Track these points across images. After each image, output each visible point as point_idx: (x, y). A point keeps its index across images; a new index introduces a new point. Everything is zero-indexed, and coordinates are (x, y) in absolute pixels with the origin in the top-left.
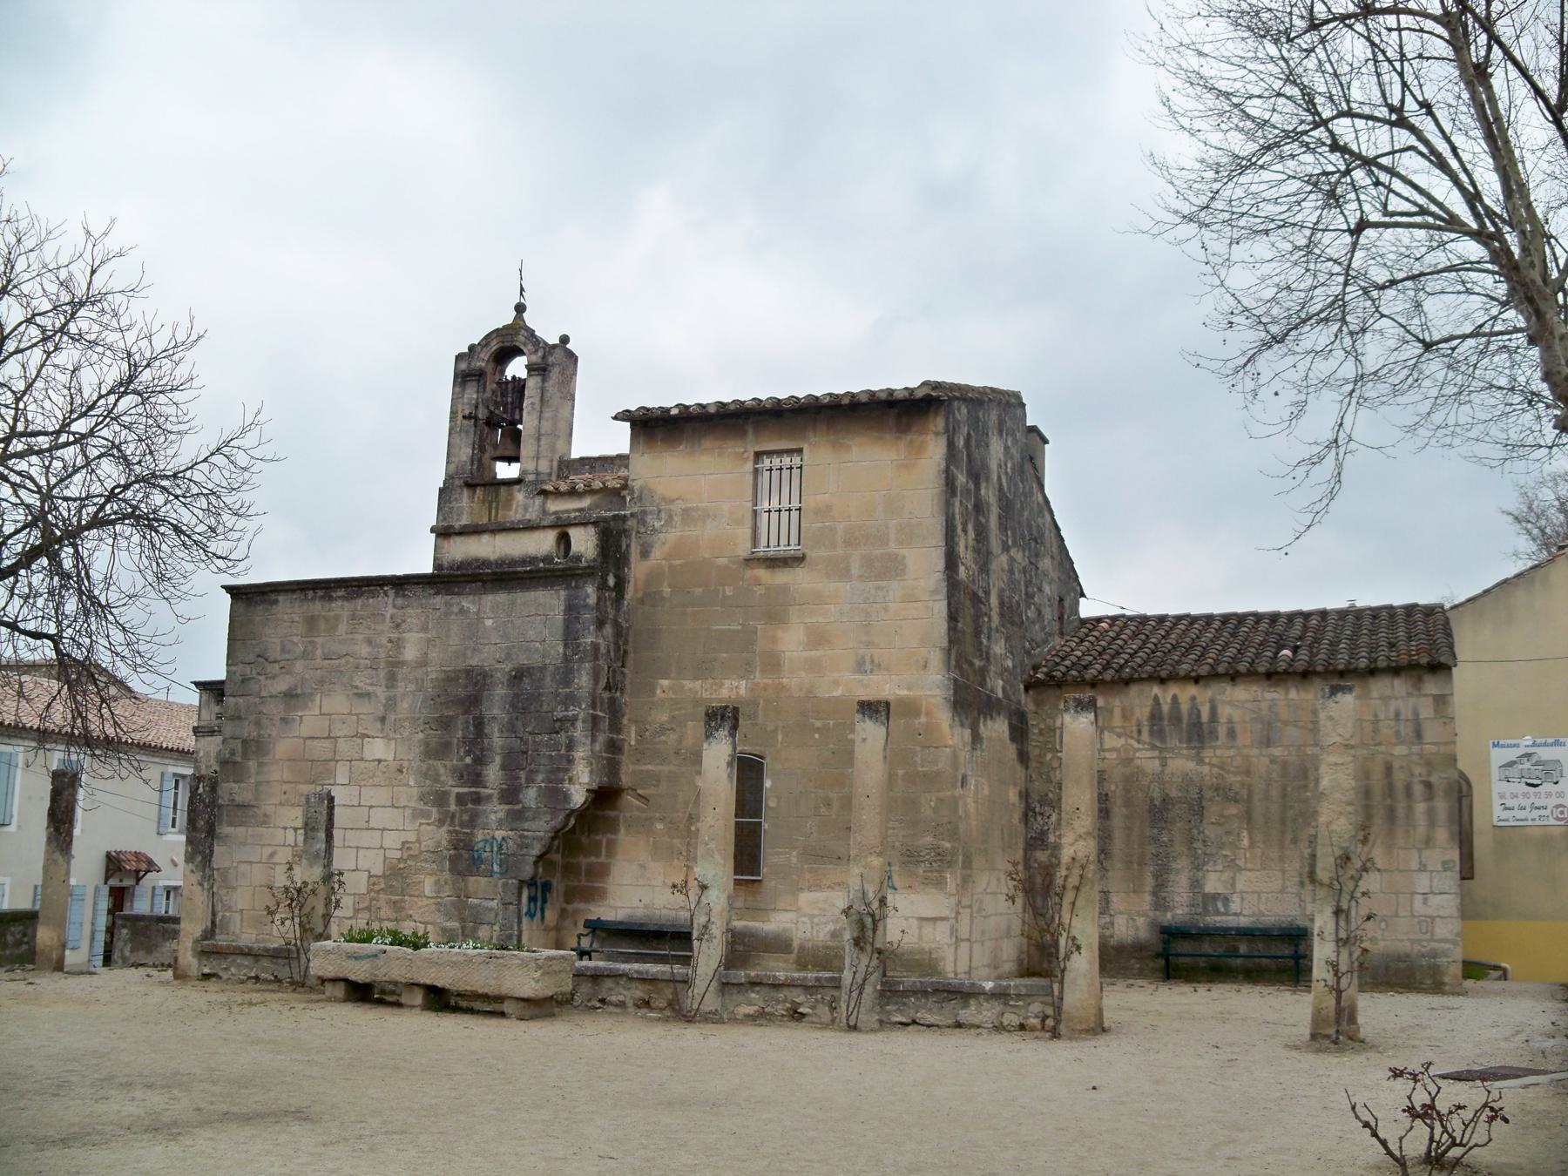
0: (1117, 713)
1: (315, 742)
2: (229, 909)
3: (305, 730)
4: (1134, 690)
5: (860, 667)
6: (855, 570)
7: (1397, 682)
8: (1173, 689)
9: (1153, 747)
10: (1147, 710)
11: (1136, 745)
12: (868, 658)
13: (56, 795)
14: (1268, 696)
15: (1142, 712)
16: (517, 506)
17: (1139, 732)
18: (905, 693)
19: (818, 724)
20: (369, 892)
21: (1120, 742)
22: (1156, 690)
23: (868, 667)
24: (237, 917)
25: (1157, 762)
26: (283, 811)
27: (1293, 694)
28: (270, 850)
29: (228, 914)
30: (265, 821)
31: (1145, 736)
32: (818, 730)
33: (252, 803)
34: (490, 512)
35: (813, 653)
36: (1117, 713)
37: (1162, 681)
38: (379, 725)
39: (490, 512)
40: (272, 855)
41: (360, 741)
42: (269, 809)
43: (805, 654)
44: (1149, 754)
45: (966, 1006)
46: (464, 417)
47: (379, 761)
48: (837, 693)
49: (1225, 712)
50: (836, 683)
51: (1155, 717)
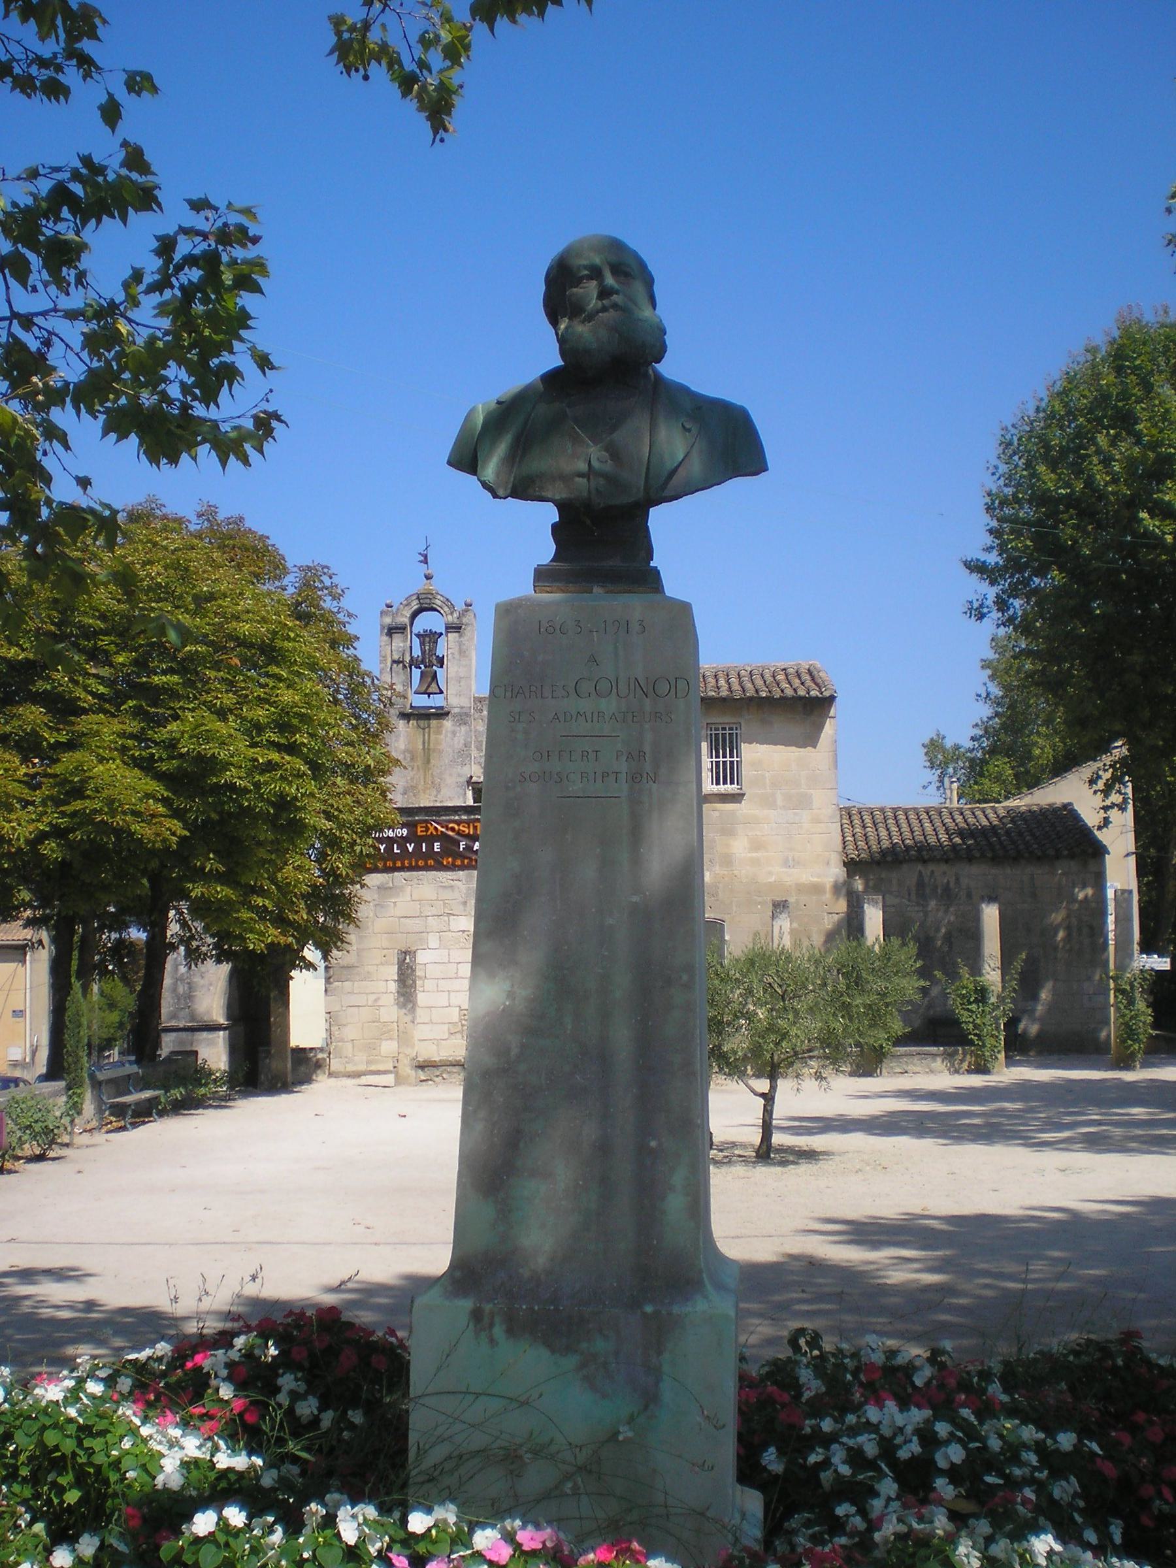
0: (894, 882)
1: (408, 920)
2: (342, 1040)
3: (398, 912)
4: (905, 867)
5: (786, 863)
6: (779, 802)
7: (1072, 863)
8: (931, 867)
9: (918, 904)
10: (914, 881)
11: (907, 903)
12: (790, 858)
13: (401, 963)
14: (993, 871)
15: (912, 881)
16: (447, 732)
17: (909, 894)
18: (816, 879)
19: (760, 899)
20: (461, 1020)
21: (897, 901)
22: (920, 867)
23: (791, 863)
24: (349, 1045)
25: (922, 914)
26: (382, 969)
27: (1008, 871)
28: (373, 997)
29: (340, 1044)
30: (367, 977)
31: (913, 897)
32: (760, 903)
33: (356, 965)
34: (424, 735)
35: (754, 855)
36: (894, 882)
37: (925, 862)
38: (461, 907)
39: (424, 735)
40: (376, 1000)
41: (446, 918)
42: (372, 969)
43: (749, 855)
44: (916, 909)
45: (935, 1061)
46: (394, 662)
47: (464, 931)
48: (772, 879)
49: (965, 881)
50: (770, 873)
51: (921, 885)
